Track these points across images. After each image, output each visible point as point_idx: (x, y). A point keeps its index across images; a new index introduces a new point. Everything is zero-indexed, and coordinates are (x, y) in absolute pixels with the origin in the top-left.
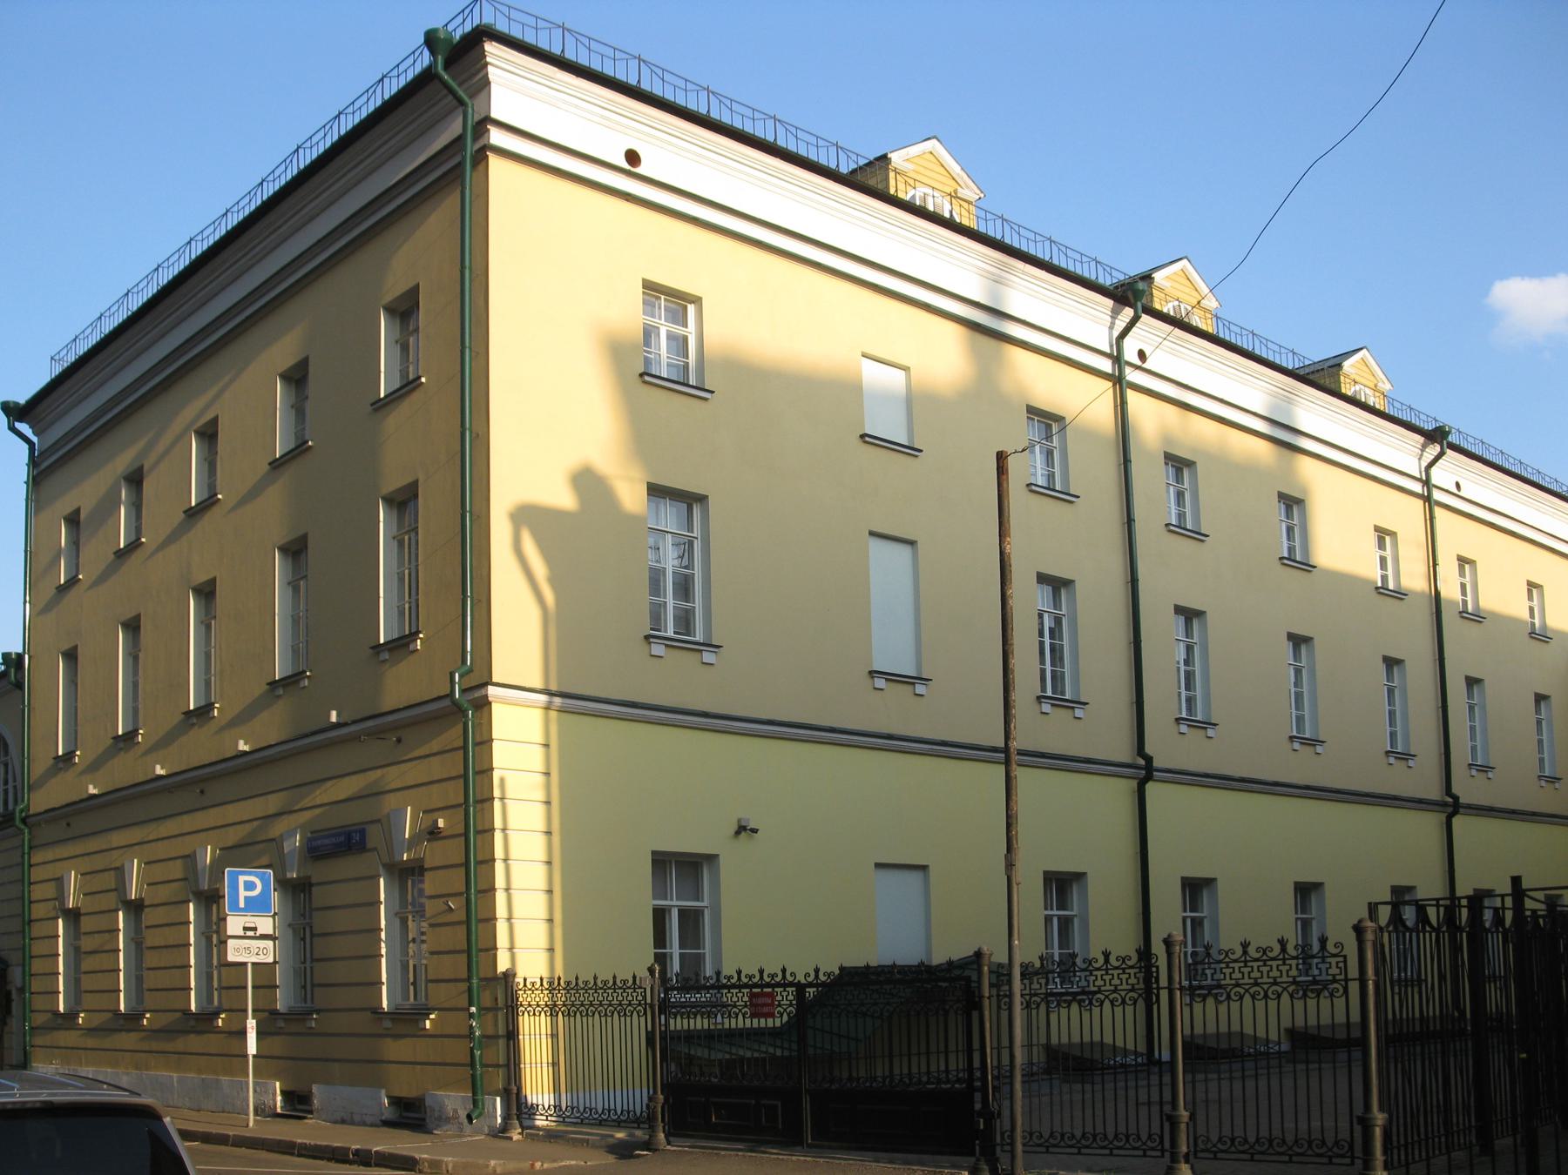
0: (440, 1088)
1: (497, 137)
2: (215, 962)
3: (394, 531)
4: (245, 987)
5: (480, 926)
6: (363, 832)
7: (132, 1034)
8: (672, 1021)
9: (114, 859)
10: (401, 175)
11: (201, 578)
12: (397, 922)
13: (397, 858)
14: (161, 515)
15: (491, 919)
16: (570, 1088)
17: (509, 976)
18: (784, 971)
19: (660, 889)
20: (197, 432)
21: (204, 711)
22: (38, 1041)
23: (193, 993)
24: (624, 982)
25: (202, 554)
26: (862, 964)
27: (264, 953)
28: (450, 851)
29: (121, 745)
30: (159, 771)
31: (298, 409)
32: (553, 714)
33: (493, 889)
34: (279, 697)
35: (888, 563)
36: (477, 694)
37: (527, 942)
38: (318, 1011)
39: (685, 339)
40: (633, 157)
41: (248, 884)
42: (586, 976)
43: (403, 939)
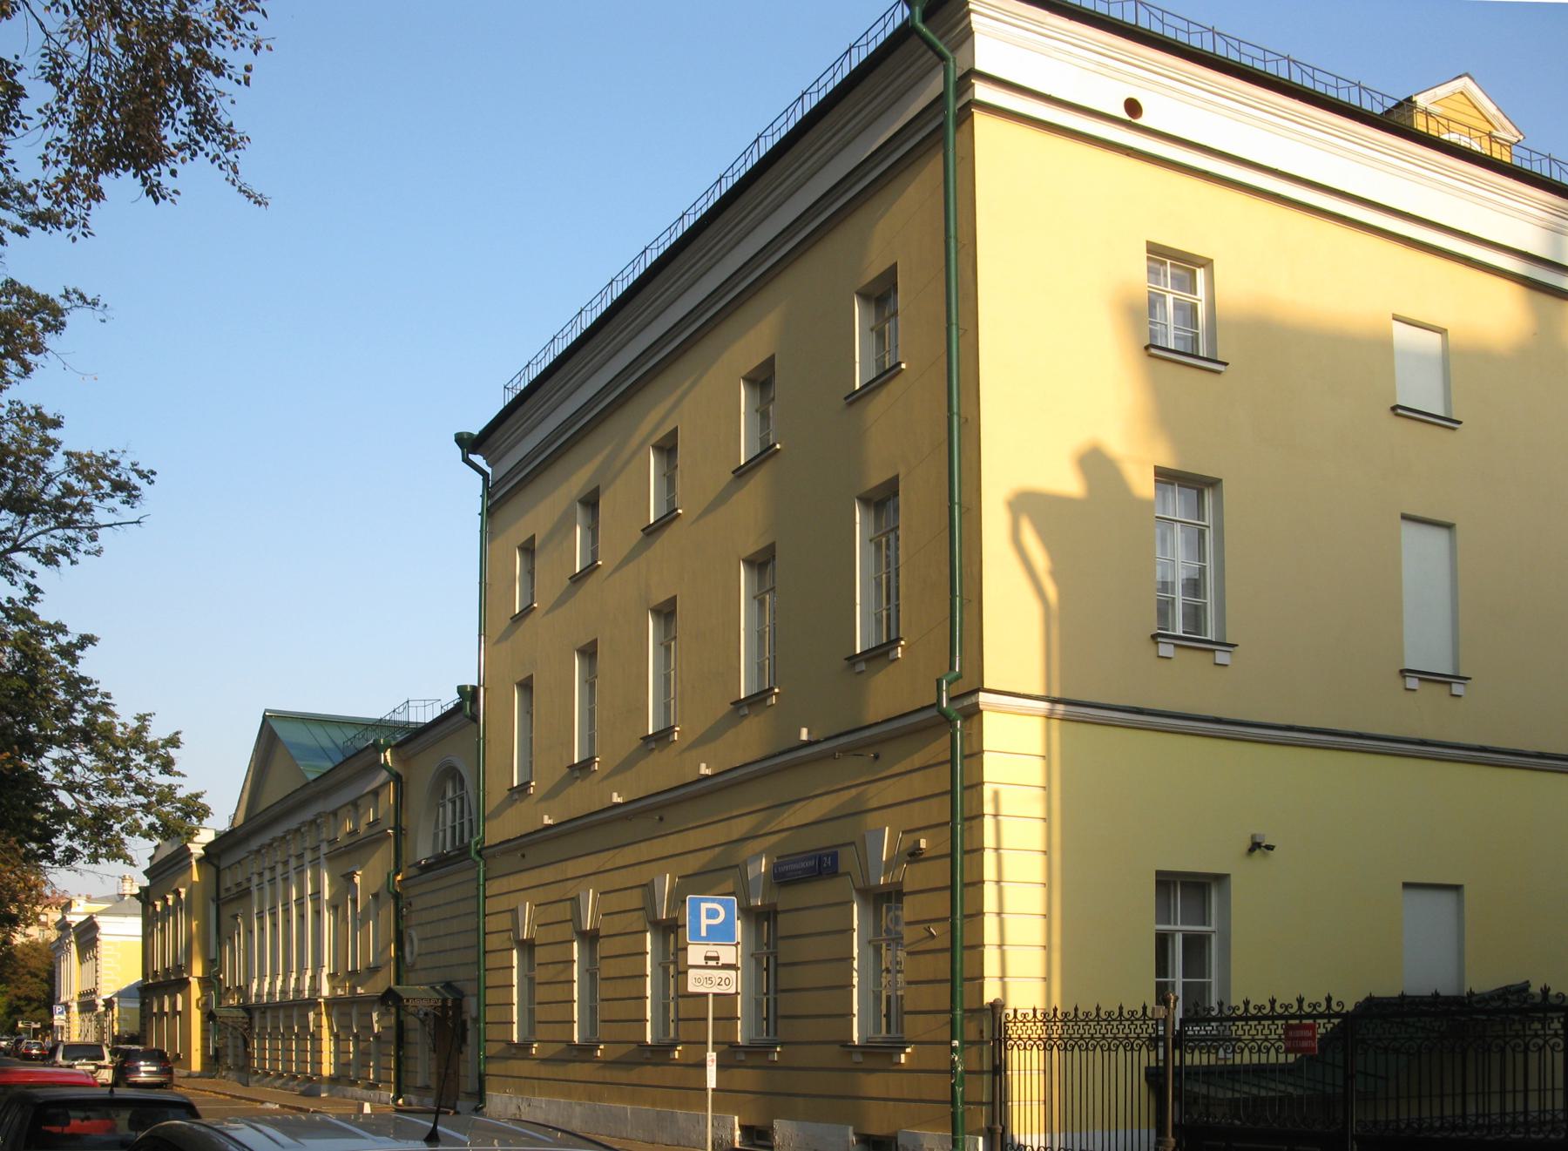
0: (913, 1127)
1: (982, 92)
2: (672, 993)
3: (872, 533)
4: (706, 1019)
5: (966, 953)
6: (835, 857)
7: (586, 1065)
8: (1188, 1057)
9: (569, 889)
10: (874, 147)
11: (660, 597)
12: (871, 951)
13: (873, 883)
14: (619, 530)
15: (978, 946)
16: (1065, 1126)
17: (997, 1007)
18: (1329, 999)
19: (1163, 913)
20: (654, 447)
21: (663, 735)
22: (492, 1068)
23: (649, 1025)
24: (1132, 1013)
25: (662, 571)
26: (1395, 993)
27: (730, 983)
28: (936, 873)
29: (577, 774)
30: (616, 799)
31: (762, 415)
32: (1055, 723)
33: (981, 913)
34: (745, 716)
35: (1422, 553)
36: (967, 702)
37: (1020, 965)
38: (782, 1044)
39: (1194, 308)
40: (1133, 107)
41: (710, 911)
42: (1087, 1006)
43: (877, 970)
